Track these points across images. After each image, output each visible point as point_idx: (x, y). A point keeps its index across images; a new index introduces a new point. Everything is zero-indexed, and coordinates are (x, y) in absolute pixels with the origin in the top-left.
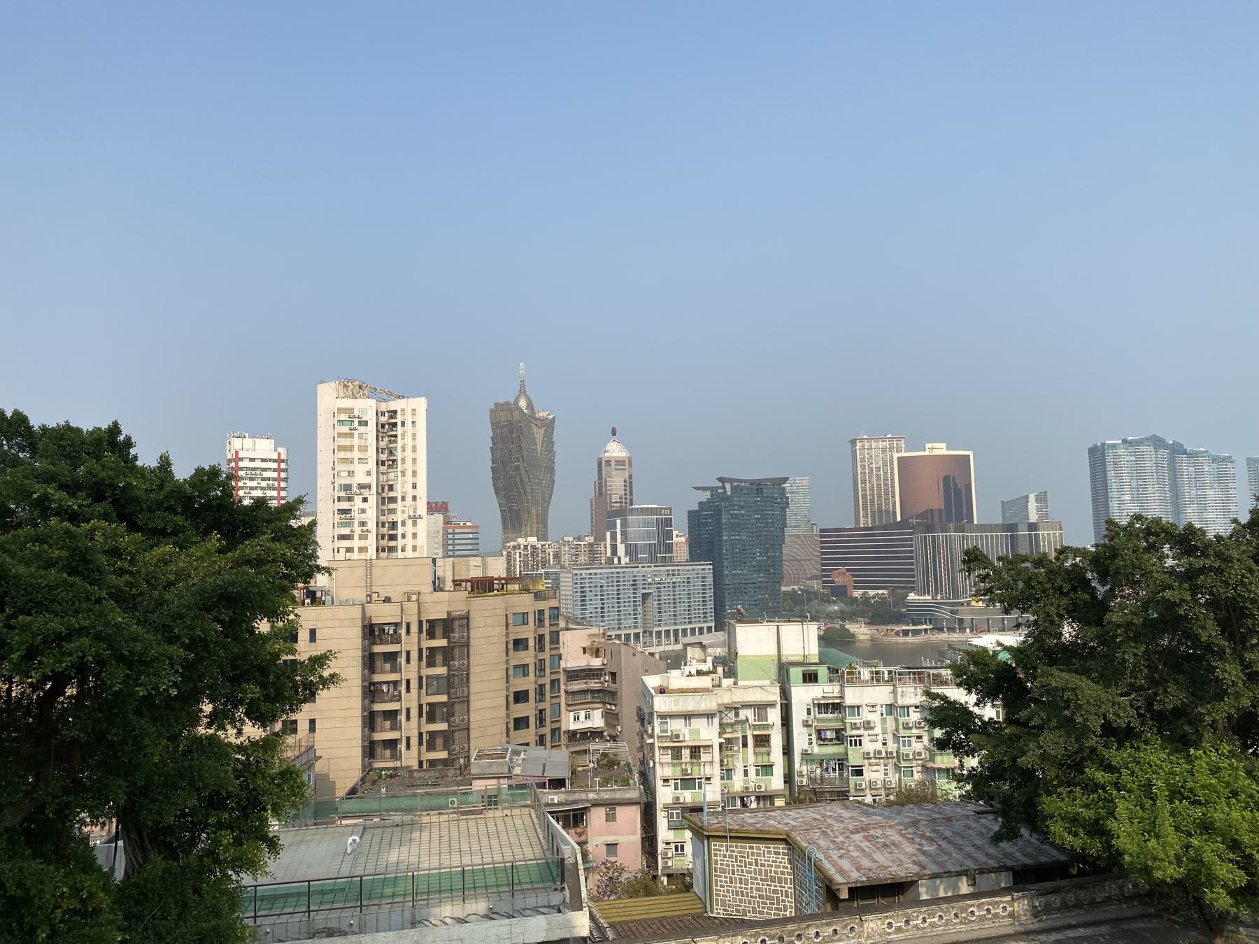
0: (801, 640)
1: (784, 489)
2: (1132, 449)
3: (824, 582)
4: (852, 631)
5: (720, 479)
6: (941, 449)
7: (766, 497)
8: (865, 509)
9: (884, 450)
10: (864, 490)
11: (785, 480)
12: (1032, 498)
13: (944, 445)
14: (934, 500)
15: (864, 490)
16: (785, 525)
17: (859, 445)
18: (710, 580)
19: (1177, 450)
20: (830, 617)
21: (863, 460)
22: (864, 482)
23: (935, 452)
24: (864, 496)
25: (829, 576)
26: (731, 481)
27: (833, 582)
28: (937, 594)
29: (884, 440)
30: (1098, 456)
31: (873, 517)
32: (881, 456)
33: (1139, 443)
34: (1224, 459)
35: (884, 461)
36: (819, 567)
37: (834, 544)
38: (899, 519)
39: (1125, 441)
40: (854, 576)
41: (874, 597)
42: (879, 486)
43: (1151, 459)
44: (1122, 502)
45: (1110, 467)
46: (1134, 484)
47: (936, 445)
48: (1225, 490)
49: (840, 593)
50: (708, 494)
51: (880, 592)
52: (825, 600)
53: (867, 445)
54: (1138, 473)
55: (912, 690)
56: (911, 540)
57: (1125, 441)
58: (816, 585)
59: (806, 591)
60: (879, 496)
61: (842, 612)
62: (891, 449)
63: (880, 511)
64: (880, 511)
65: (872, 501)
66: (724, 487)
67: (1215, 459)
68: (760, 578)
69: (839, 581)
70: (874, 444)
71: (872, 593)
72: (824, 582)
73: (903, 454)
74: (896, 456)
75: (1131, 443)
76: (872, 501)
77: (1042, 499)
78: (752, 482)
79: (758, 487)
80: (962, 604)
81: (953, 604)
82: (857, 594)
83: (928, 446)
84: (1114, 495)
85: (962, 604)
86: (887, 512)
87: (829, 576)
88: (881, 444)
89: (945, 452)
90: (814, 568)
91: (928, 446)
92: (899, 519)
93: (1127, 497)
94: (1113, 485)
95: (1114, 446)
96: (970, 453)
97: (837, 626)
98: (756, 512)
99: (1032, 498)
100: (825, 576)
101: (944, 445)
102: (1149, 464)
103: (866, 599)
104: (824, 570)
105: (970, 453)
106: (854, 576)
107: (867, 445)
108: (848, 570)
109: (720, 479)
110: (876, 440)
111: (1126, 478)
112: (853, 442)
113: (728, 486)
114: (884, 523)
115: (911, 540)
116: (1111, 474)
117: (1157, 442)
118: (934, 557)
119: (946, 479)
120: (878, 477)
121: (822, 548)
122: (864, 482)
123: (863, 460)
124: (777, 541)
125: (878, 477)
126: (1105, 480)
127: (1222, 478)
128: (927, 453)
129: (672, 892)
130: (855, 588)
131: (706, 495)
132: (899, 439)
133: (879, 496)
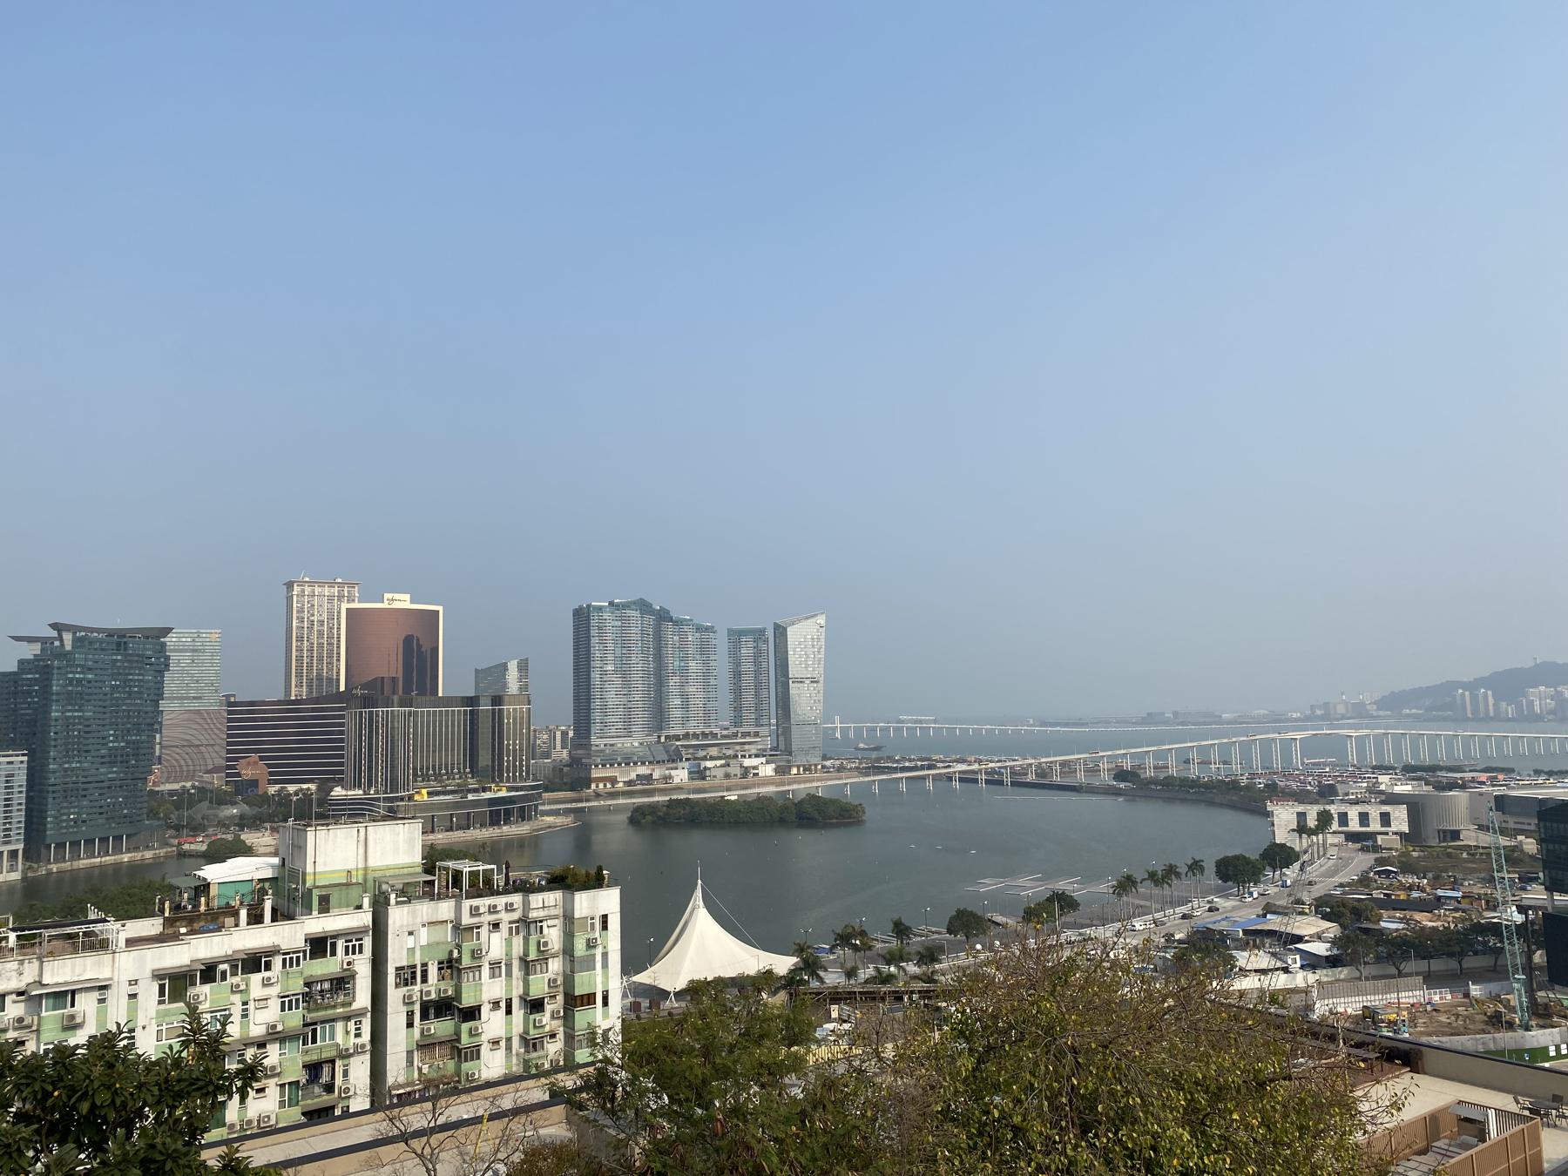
0: (396, 846)
1: (164, 644)
2: (618, 613)
3: (228, 775)
4: (248, 842)
5: (54, 626)
6: (403, 601)
7: (136, 656)
8: (299, 675)
9: (331, 599)
10: (300, 650)
11: (167, 631)
12: (513, 666)
13: (407, 597)
14: (387, 663)
15: (300, 650)
16: (160, 696)
17: (296, 590)
18: (21, 778)
19: (663, 616)
20: (223, 824)
21: (301, 610)
22: (300, 639)
23: (396, 605)
24: (300, 659)
25: (233, 767)
26: (73, 629)
27: (239, 775)
28: (370, 786)
29: (331, 585)
30: (582, 618)
31: (310, 686)
32: (326, 608)
33: (625, 606)
34: (707, 629)
35: (330, 612)
36: (224, 755)
37: (246, 723)
38: (342, 688)
39: (611, 604)
40: (269, 766)
41: (296, 794)
42: (320, 645)
43: (637, 624)
44: (604, 673)
45: (594, 632)
46: (618, 651)
47: (397, 596)
48: (706, 663)
49: (245, 789)
50: (36, 648)
51: (305, 786)
52: (221, 799)
53: (308, 590)
54: (624, 641)
55: (15, 965)
56: (342, 717)
57: (611, 604)
58: (217, 781)
59: (201, 790)
60: (320, 659)
61: (242, 817)
62: (340, 597)
63: (320, 677)
64: (320, 677)
65: (310, 666)
66: (61, 640)
67: (699, 629)
68: (114, 773)
69: (248, 773)
70: (317, 590)
71: (292, 788)
72: (228, 775)
73: (356, 605)
74: (345, 606)
75: (618, 605)
76: (310, 666)
77: (523, 667)
78: (110, 633)
79: (119, 639)
80: (402, 799)
81: (391, 800)
82: (273, 789)
83: (387, 596)
84: (596, 664)
85: (402, 799)
86: (330, 680)
87: (233, 767)
88: (326, 591)
89: (408, 605)
90: (217, 757)
91: (387, 596)
92: (342, 688)
93: (610, 668)
94: (596, 652)
95: (600, 609)
96: (440, 609)
97: (230, 837)
98: (113, 677)
99: (513, 666)
100: (230, 770)
101: (407, 597)
102: (635, 632)
103: (283, 799)
104: (228, 759)
105: (440, 609)
106: (269, 766)
107: (308, 590)
108: (261, 759)
109: (54, 626)
110: (322, 585)
111: (610, 646)
112: (290, 585)
113: (68, 638)
114: (325, 697)
115: (342, 717)
116: (594, 641)
117: (644, 607)
118: (370, 738)
119: (408, 640)
120: (321, 633)
121: (229, 728)
122: (300, 639)
123: (301, 610)
124: (151, 722)
125: (321, 633)
126: (588, 646)
127: (704, 649)
128: (385, 605)
129: (1117, 792)
130: (270, 782)
131: (30, 651)
132: (352, 585)
133: (320, 659)
